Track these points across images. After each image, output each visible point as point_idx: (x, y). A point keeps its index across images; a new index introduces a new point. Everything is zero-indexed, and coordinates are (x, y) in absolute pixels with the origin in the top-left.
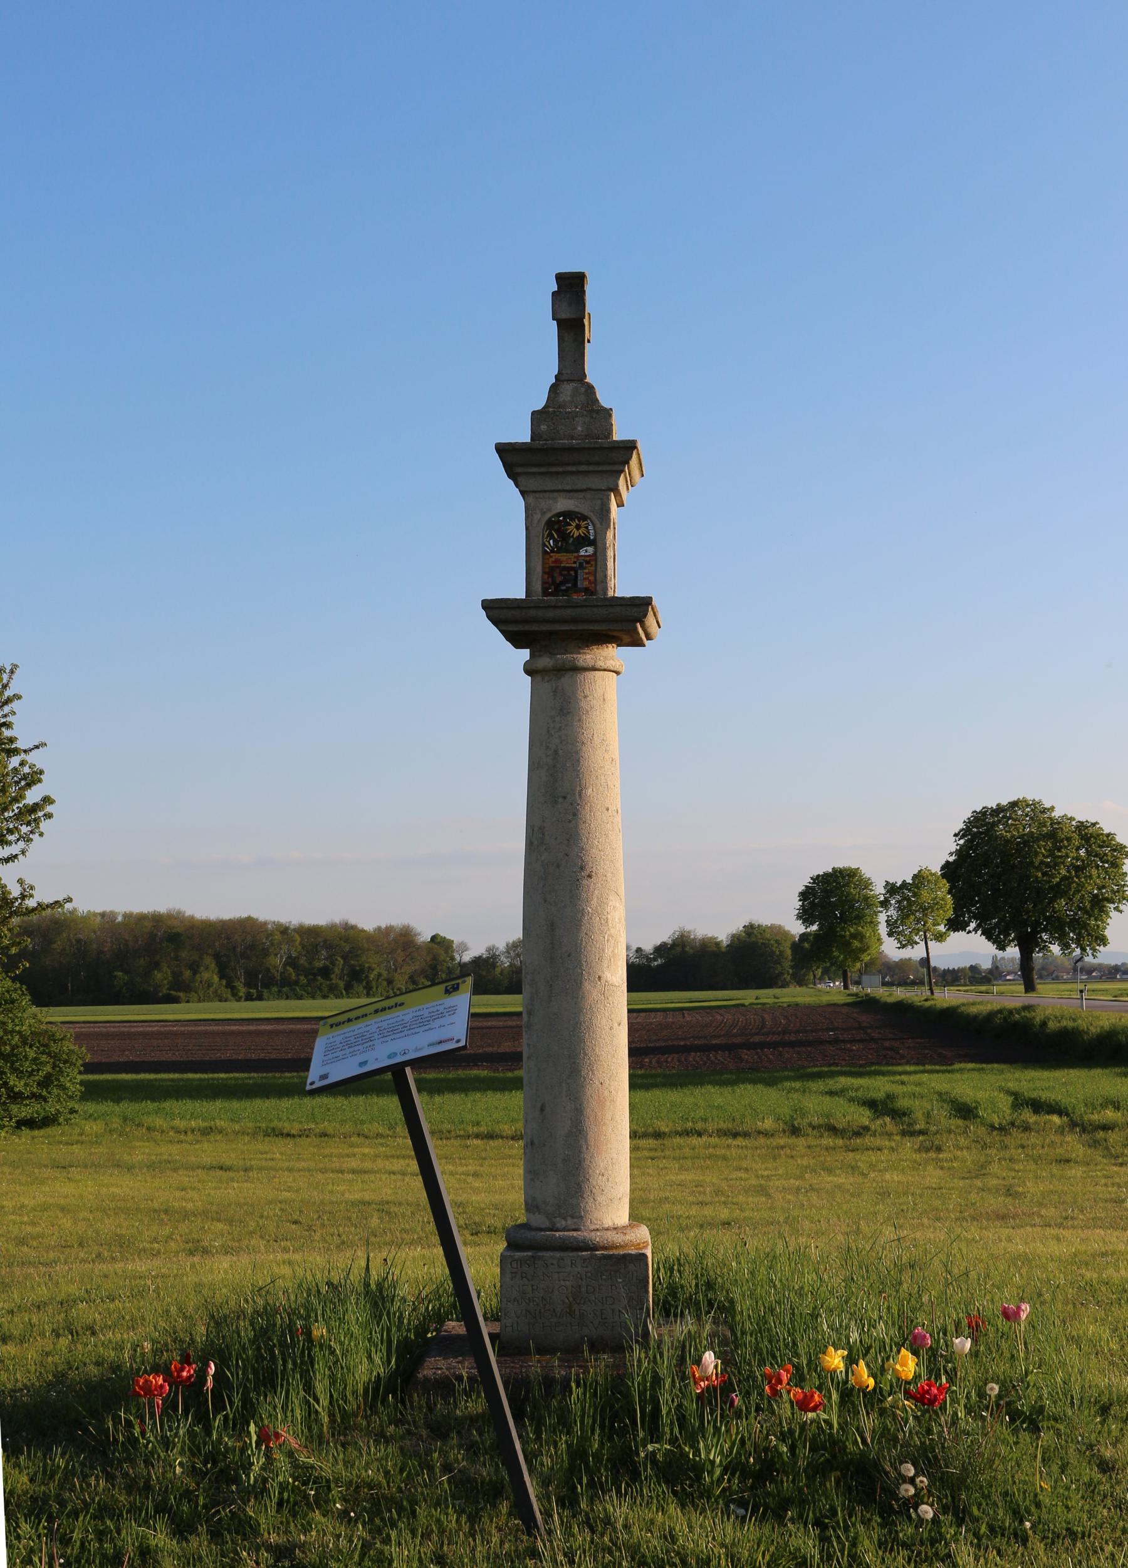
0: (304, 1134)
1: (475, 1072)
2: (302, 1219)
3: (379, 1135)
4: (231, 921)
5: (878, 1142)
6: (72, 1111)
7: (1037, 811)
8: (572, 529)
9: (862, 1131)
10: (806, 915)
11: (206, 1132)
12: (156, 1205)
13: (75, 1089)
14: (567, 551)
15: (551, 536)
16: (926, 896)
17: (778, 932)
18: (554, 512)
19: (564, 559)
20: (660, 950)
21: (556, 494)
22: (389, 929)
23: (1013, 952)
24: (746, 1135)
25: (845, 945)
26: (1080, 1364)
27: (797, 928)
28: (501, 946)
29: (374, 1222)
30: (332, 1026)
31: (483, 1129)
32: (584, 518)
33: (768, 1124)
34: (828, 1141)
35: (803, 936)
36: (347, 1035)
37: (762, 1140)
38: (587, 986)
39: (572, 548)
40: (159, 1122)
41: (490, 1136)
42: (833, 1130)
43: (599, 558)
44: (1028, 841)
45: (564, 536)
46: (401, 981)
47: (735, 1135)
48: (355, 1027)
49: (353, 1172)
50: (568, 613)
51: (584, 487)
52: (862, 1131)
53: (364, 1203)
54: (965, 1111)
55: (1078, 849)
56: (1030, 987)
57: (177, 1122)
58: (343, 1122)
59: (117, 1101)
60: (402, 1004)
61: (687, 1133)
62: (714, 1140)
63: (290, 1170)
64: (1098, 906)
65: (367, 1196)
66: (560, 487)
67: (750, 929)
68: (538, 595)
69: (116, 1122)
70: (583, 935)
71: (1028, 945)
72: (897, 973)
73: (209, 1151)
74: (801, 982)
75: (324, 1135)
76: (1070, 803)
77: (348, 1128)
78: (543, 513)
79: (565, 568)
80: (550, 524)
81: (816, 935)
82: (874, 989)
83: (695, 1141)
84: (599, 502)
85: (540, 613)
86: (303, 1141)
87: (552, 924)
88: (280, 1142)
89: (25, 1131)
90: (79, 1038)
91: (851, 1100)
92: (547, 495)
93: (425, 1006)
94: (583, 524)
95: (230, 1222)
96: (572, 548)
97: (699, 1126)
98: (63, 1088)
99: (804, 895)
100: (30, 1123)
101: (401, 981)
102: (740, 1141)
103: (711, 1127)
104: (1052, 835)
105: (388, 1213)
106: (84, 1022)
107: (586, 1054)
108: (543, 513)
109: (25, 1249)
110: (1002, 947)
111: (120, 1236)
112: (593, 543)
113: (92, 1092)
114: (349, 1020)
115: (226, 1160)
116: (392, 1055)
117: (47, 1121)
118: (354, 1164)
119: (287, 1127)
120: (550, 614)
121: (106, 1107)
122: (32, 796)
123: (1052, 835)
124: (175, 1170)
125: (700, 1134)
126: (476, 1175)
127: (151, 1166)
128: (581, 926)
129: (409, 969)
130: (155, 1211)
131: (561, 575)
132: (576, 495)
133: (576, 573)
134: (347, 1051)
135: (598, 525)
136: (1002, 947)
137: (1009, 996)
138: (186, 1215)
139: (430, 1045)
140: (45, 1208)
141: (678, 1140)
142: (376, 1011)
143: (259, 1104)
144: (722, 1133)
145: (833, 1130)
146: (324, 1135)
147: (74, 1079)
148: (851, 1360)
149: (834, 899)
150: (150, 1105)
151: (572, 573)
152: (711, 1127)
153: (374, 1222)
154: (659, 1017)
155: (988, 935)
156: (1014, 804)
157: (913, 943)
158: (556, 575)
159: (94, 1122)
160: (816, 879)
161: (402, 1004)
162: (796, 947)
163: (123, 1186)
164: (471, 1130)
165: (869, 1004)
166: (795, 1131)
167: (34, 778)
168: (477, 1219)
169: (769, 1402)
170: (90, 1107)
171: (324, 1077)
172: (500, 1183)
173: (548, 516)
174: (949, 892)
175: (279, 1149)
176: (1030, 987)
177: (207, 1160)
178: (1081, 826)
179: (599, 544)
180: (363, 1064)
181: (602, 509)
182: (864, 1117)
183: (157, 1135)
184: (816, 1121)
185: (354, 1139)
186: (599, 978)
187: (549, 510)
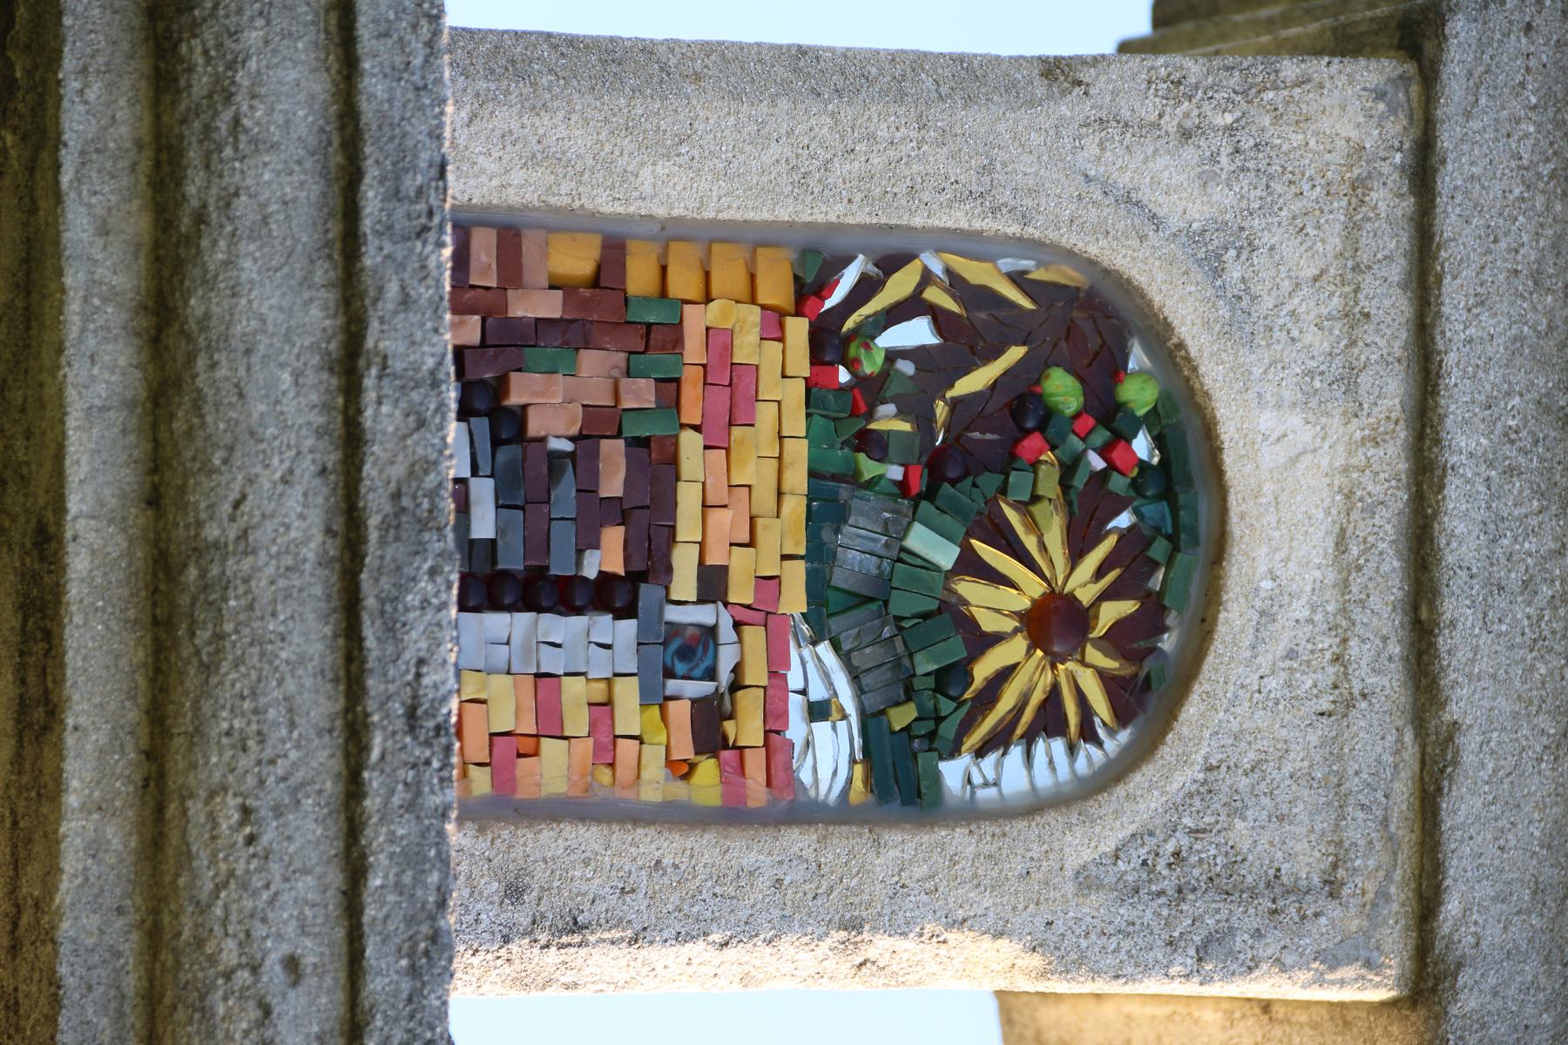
8: (1046, 559)
14: (828, 501)
15: (966, 336)
18: (1214, 374)
19: (754, 470)
21: (1389, 392)
32: (1147, 695)
39: (857, 554)
43: (751, 852)
45: (965, 469)
50: (275, 510)
51: (1465, 702)
55: (269, 183)
66: (1464, 441)
68: (490, 162)
78: (1210, 252)
79: (656, 463)
80: (1091, 322)
84: (1305, 860)
85: (271, 180)
92: (1389, 304)
94: (1087, 676)
96: (857, 554)
108: (1210, 252)
112: (898, 778)
120: (267, 301)
131: (599, 425)
132: (1382, 612)
133: (610, 595)
135: (1083, 842)
148: (225, 431)
151: (607, 556)
158: (595, 370)
173: (1184, 307)
174: (197, 375)
179: (901, 850)
181: (1226, 885)
187: (1242, 320)
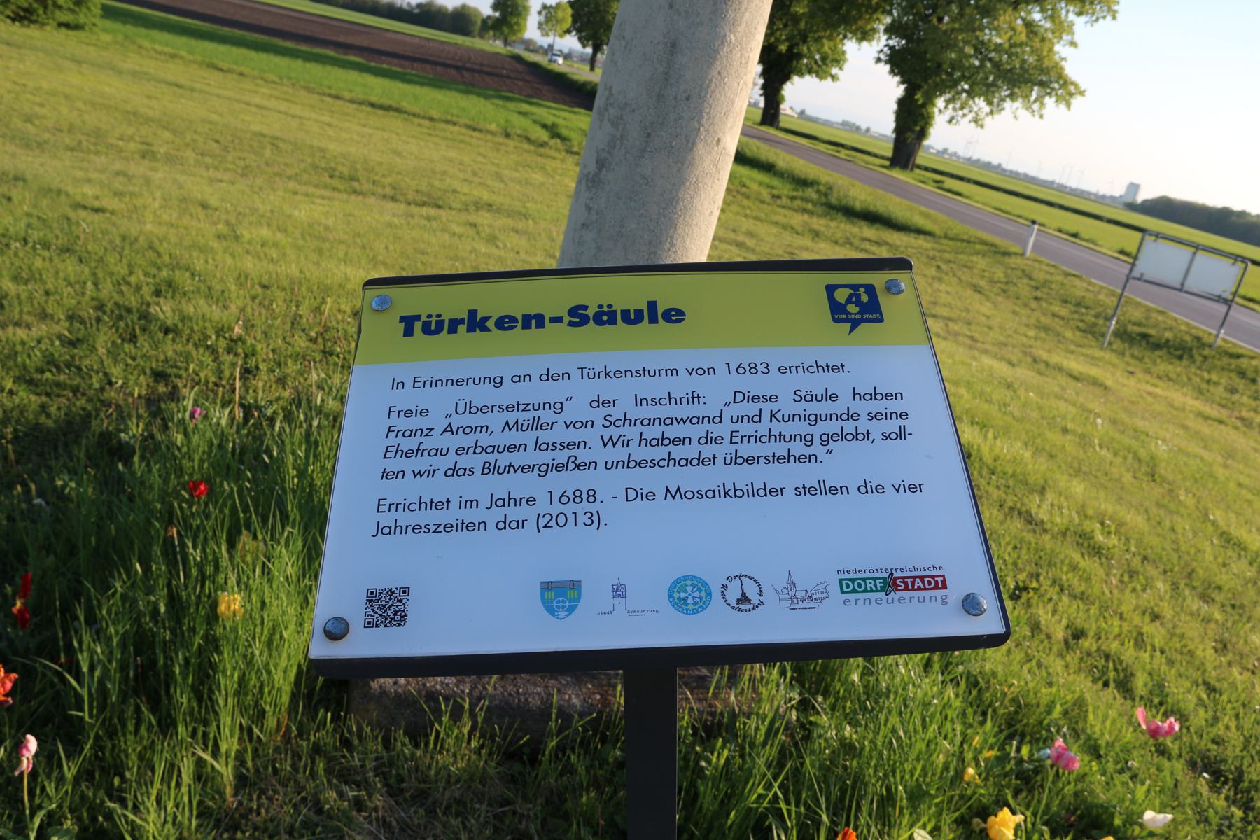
0: (229, 71)
2: (221, 139)
3: (274, 82)
5: (553, 153)
6: (94, 25)
9: (543, 145)
11: (173, 56)
12: (129, 108)
16: (560, 14)
17: (476, 11)
23: (589, 50)
24: (480, 131)
25: (511, 26)
29: (267, 153)
30: (409, 323)
31: (333, 92)
33: (493, 127)
34: (526, 146)
35: (489, 17)
36: (482, 395)
37: (489, 137)
38: (700, 148)
40: (146, 44)
41: (337, 97)
42: (528, 139)
47: (475, 130)
48: (505, 366)
49: (257, 106)
52: (543, 145)
53: (263, 135)
57: (157, 47)
58: (253, 69)
59: (125, 23)
60: (674, 316)
61: (447, 122)
62: (463, 130)
63: (218, 96)
65: (265, 131)
67: (464, 7)
69: (120, 37)
70: (714, 73)
71: (597, 49)
72: (529, 45)
73: (174, 71)
74: (481, 37)
75: (241, 74)
77: (256, 73)
81: (497, 19)
82: (518, 50)
83: (451, 128)
86: (230, 76)
87: (674, 45)
88: (216, 73)
89: (63, 30)
91: (535, 122)
93: (777, 356)
95: (174, 132)
97: (455, 119)
98: (89, 9)
100: (67, 26)
102: (476, 134)
105: (277, 147)
107: (673, 245)
109: (29, 126)
110: (584, 46)
111: (99, 129)
114: (475, 323)
115: (182, 81)
116: (688, 594)
117: (77, 27)
118: (257, 100)
119: (221, 64)
121: (117, 26)
124: (148, 80)
125: (455, 124)
126: (329, 125)
127: (134, 74)
128: (715, 59)
130: (128, 112)
134: (481, 487)
136: (584, 46)
138: (148, 120)
139: (852, 585)
140: (54, 93)
141: (443, 125)
142: (578, 316)
144: (468, 127)
145: (528, 139)
146: (241, 74)
150: (143, 31)
152: (462, 121)
153: (267, 153)
154: (408, 38)
155: (580, 39)
157: (547, 35)
159: (107, 33)
161: (674, 316)
162: (485, 21)
163: (114, 87)
164: (328, 91)
165: (518, 59)
166: (507, 135)
168: (333, 165)
170: (108, 24)
171: (388, 607)
172: (344, 135)
177: (170, 78)
180: (561, 594)
182: (544, 135)
183: (144, 52)
184: (519, 132)
185: (259, 82)
186: (719, 141)
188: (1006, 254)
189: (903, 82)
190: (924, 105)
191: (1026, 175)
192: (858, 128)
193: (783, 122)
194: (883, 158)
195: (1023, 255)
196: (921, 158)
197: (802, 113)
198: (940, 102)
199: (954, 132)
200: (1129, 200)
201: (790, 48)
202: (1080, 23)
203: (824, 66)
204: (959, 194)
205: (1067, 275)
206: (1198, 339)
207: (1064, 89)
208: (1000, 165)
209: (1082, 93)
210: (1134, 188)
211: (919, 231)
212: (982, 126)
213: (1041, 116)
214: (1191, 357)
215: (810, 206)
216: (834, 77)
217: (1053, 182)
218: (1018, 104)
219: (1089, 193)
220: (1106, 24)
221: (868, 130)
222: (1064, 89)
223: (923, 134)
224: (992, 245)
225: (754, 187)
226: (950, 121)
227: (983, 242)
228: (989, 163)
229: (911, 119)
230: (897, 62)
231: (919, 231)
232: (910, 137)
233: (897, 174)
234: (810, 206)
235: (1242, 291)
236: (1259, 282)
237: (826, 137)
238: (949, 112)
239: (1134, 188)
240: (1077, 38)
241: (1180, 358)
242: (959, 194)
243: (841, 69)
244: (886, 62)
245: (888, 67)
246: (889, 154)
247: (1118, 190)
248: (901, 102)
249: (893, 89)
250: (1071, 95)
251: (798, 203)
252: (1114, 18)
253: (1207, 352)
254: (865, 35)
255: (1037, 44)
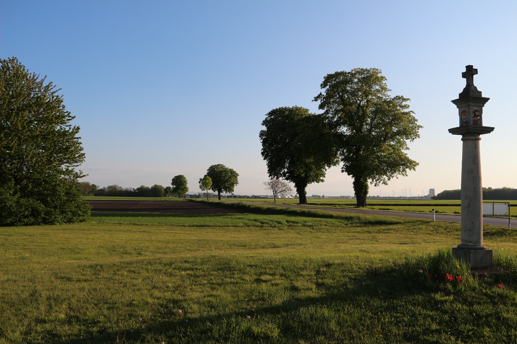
1: (145, 213)
4: (441, 193)
7: (222, 166)
10: (173, 184)
13: (89, 214)
20: (138, 189)
22: (84, 183)
26: (516, 263)
27: (172, 186)
28: (106, 187)
33: (241, 225)
44: (221, 172)
46: (86, 193)
54: (279, 223)
56: (219, 199)
64: (233, 184)
67: (155, 186)
76: (228, 165)
90: (91, 204)
99: (173, 180)
100: (81, 221)
101: (86, 193)
103: (230, 225)
104: (225, 171)
106: (384, 209)
110: (214, 191)
113: (93, 215)
117: (84, 220)
121: (95, 218)
122: (82, 152)
123: (225, 171)
129: (88, 191)
136: (214, 191)
137: (217, 200)
143: (129, 218)
144: (189, 226)
147: (89, 212)
149: (179, 182)
152: (230, 225)
156: (218, 165)
159: (94, 221)
160: (175, 177)
167: (82, 149)
169: (462, 268)
170: (94, 218)
175: (136, 228)
176: (219, 199)
178: (230, 169)
188: (428, 222)
189: (353, 177)
190: (364, 183)
191: (389, 197)
192: (319, 197)
193: (308, 201)
194: (354, 205)
195: (433, 221)
196: (368, 201)
197: (323, 196)
198: (369, 180)
199: (375, 190)
200: (432, 196)
201: (305, 175)
202: (408, 142)
203: (317, 178)
204: (389, 209)
205: (451, 223)
206: (504, 229)
207: (409, 164)
208: (378, 196)
209: (418, 164)
210: (432, 191)
211: (397, 223)
212: (387, 184)
213: (407, 175)
214: (505, 234)
215: (358, 225)
216: (322, 181)
217: (400, 197)
218: (397, 173)
219: (416, 197)
220: (417, 140)
221: (323, 196)
222: (409, 164)
223: (366, 192)
224: (421, 221)
225: (336, 223)
226: (375, 186)
227: (418, 221)
228: (374, 197)
229: (360, 188)
230: (349, 170)
231: (397, 223)
232: (362, 194)
233: (361, 208)
234: (358, 225)
235: (511, 214)
236: (515, 211)
237: (319, 203)
238: (375, 182)
239: (432, 191)
240: (408, 146)
241: (502, 235)
242: (389, 209)
243: (324, 177)
244: (346, 171)
245: (346, 173)
246: (356, 203)
247: (427, 193)
248: (354, 183)
249: (350, 180)
250: (414, 166)
251: (354, 225)
252: (419, 137)
253: (508, 232)
254: (330, 163)
255: (397, 152)
